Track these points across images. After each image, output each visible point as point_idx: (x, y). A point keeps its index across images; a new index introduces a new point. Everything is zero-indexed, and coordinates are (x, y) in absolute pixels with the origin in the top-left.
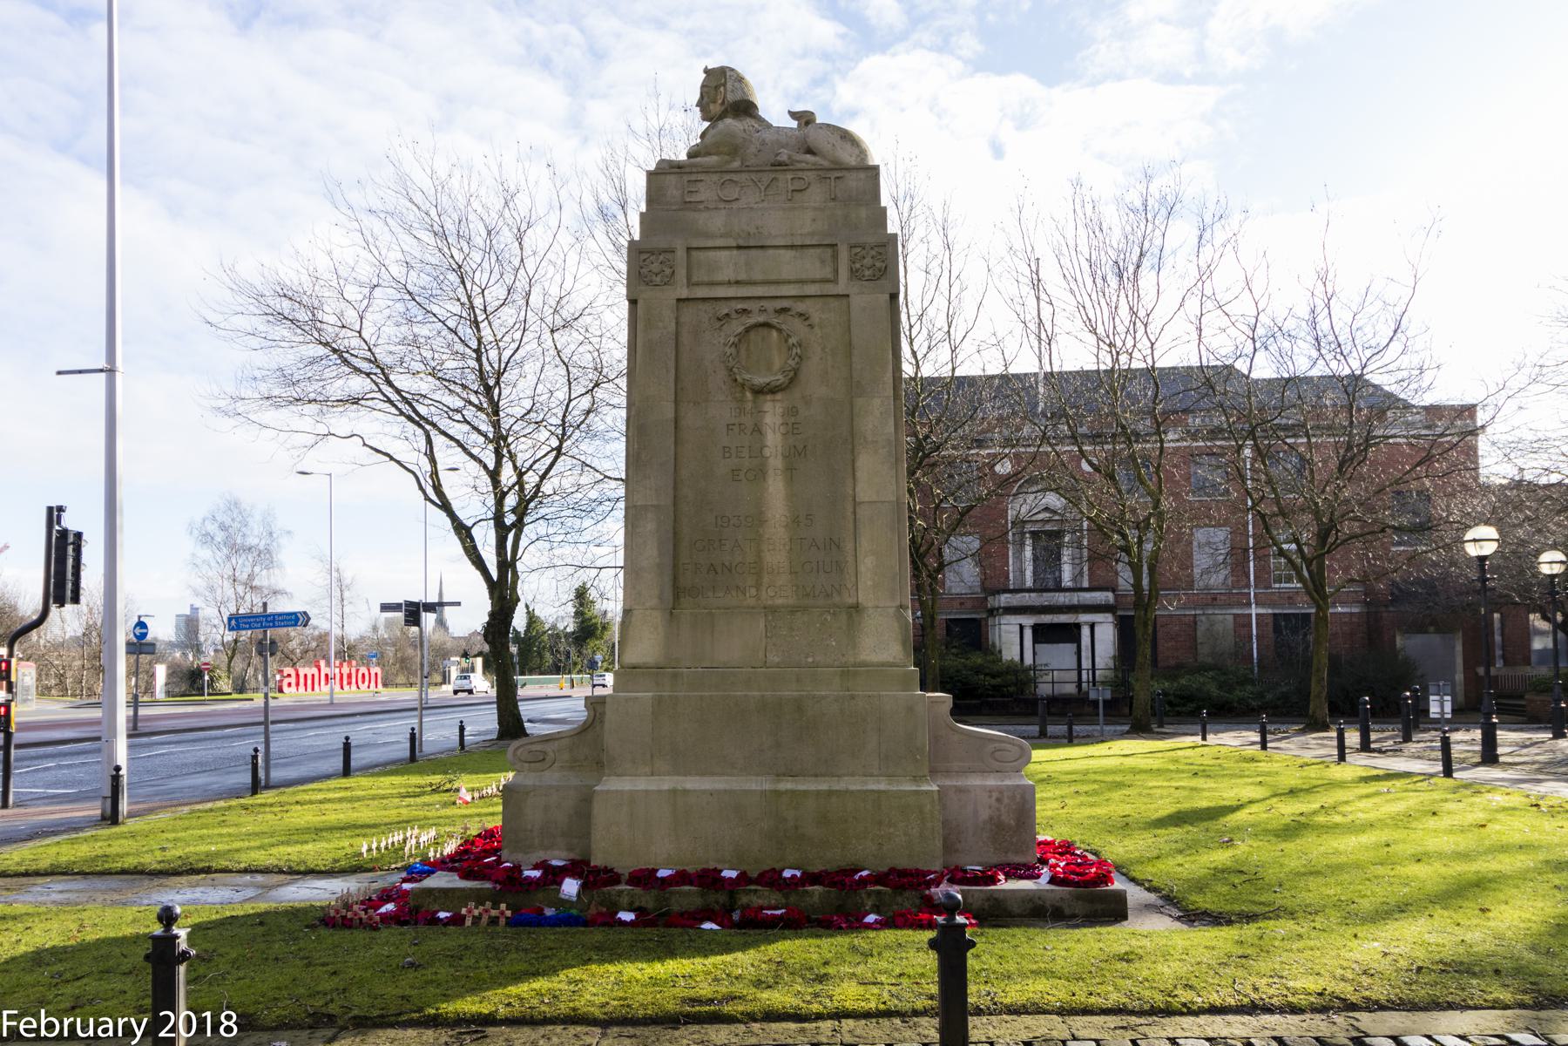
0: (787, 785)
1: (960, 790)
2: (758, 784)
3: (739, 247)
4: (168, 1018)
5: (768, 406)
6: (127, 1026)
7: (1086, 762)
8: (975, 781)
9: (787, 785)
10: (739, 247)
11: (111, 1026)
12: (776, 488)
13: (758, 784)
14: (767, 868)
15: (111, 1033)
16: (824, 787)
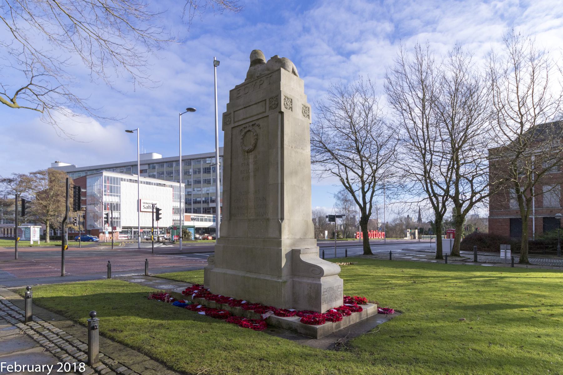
0: (248, 275)
1: (300, 283)
2: (241, 273)
3: (245, 108)
4: (60, 365)
5: (250, 157)
6: (46, 368)
7: (543, 279)
8: (305, 280)
9: (248, 275)
10: (245, 108)
11: (40, 368)
12: (252, 181)
13: (241, 273)
14: (221, 106)
15: (40, 370)
16: (255, 277)
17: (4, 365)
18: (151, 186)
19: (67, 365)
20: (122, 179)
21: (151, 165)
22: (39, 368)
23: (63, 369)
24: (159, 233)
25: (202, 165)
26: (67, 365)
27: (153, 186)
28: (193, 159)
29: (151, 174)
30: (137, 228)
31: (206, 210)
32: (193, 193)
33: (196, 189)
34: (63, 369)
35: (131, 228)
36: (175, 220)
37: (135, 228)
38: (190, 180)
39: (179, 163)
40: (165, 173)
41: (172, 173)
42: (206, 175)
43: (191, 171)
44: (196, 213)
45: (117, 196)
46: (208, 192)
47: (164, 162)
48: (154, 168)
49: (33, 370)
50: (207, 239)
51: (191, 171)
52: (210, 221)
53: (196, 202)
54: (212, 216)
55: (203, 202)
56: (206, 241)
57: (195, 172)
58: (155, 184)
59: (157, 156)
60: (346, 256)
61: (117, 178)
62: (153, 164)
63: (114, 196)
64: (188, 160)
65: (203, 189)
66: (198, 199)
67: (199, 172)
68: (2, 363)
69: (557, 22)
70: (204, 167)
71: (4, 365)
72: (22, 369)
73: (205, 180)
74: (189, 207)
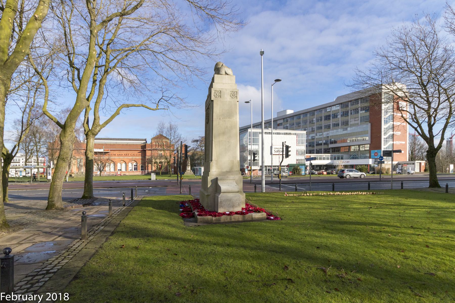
11: (32, 297)
15: (32, 299)
17: (3, 295)
18: (280, 135)
19: (54, 295)
21: (285, 119)
23: (51, 298)
24: (286, 169)
25: (323, 114)
26: (54, 295)
27: (282, 135)
28: (316, 110)
29: (285, 126)
30: (271, 166)
31: (326, 150)
32: (317, 137)
33: (318, 134)
34: (51, 298)
36: (298, 160)
37: (269, 166)
38: (313, 127)
39: (271, 124)
40: (295, 124)
41: (300, 123)
42: (327, 121)
43: (315, 119)
45: (257, 145)
47: (294, 116)
48: (287, 121)
50: (322, 174)
51: (315, 119)
52: (328, 159)
53: (318, 144)
54: (330, 155)
55: (324, 144)
56: (321, 175)
57: (318, 120)
59: (290, 112)
60: (402, 188)
62: (287, 118)
63: (255, 145)
64: (312, 111)
65: (324, 133)
66: (320, 142)
67: (321, 120)
68: (1, 293)
71: (3, 295)
72: (18, 298)
74: (313, 149)
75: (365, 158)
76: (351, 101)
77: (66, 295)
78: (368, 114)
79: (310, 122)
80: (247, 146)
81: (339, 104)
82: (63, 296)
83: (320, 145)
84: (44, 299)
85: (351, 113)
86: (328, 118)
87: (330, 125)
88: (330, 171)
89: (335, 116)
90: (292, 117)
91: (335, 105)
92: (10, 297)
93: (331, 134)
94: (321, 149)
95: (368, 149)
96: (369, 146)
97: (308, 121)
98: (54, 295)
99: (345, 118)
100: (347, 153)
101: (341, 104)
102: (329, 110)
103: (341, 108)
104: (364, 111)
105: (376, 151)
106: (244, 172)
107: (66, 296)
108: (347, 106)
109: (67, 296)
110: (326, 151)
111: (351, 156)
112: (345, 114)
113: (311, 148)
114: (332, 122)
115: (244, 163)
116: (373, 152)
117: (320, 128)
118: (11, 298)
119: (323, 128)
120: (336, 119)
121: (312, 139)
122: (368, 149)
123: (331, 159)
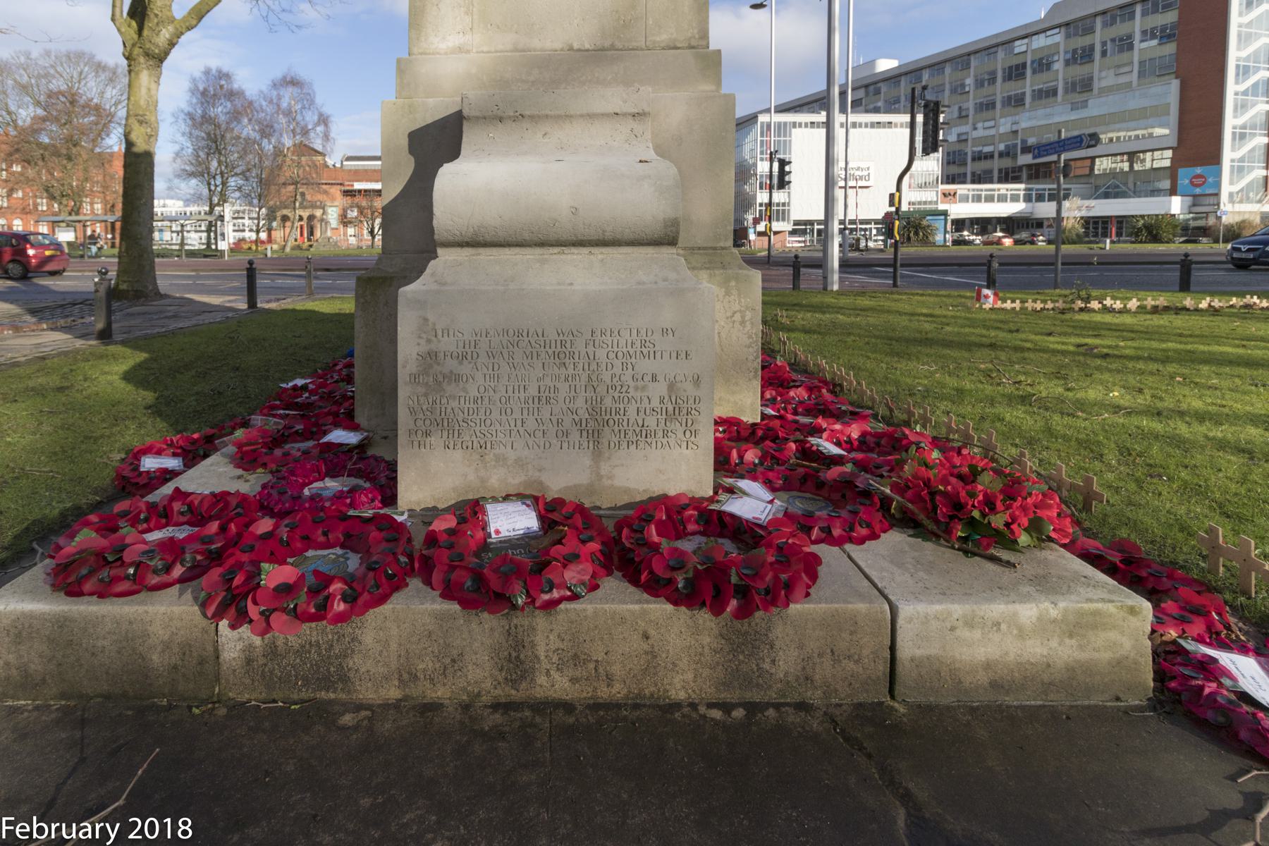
11: (89, 830)
15: (90, 836)
17: (8, 823)
19: (152, 823)
20: (794, 125)
21: (871, 88)
22: (88, 830)
23: (141, 832)
24: (874, 232)
25: (1001, 60)
26: (152, 823)
27: (863, 130)
28: (976, 52)
31: (1007, 174)
32: (975, 134)
33: (980, 125)
34: (141, 832)
35: (811, 223)
38: (965, 106)
42: (1012, 84)
43: (969, 81)
44: (979, 182)
46: (1015, 128)
47: (900, 75)
48: (878, 92)
49: (74, 835)
51: (969, 81)
52: (1015, 199)
54: (1022, 186)
55: (1001, 155)
57: (979, 84)
58: (866, 126)
59: (885, 65)
61: (785, 124)
62: (876, 83)
64: (961, 56)
67: (993, 80)
68: (4, 819)
69: (3, 353)
70: (1007, 65)
71: (8, 823)
73: (1009, 98)
74: (961, 170)
75: (1155, 192)
76: (1104, 13)
77: (185, 823)
78: (1171, 48)
79: (954, 91)
80: (755, 165)
81: (1059, 26)
82: (175, 828)
83: (986, 158)
84: (122, 835)
85: (1104, 53)
86: (1016, 72)
87: (1024, 94)
88: (1024, 235)
89: (1043, 65)
90: (892, 78)
91: (1044, 31)
92: (28, 830)
93: (1023, 125)
94: (991, 171)
95: (1167, 163)
96: (1169, 153)
97: (947, 87)
98: (152, 824)
99: (1079, 71)
100: (1083, 180)
101: (1067, 24)
102: (1024, 48)
103: (1068, 36)
104: (1155, 42)
105: (1199, 170)
106: (746, 236)
107: (186, 827)
108: (1090, 30)
109: (187, 828)
110: (1008, 176)
111: (1097, 188)
112: (1085, 55)
113: (955, 170)
114: (1029, 85)
115: (746, 212)
116: (1184, 176)
117: (991, 106)
118: (31, 834)
119: (998, 105)
120: (1045, 76)
121: (959, 141)
122: (1167, 163)
123: (1028, 199)
